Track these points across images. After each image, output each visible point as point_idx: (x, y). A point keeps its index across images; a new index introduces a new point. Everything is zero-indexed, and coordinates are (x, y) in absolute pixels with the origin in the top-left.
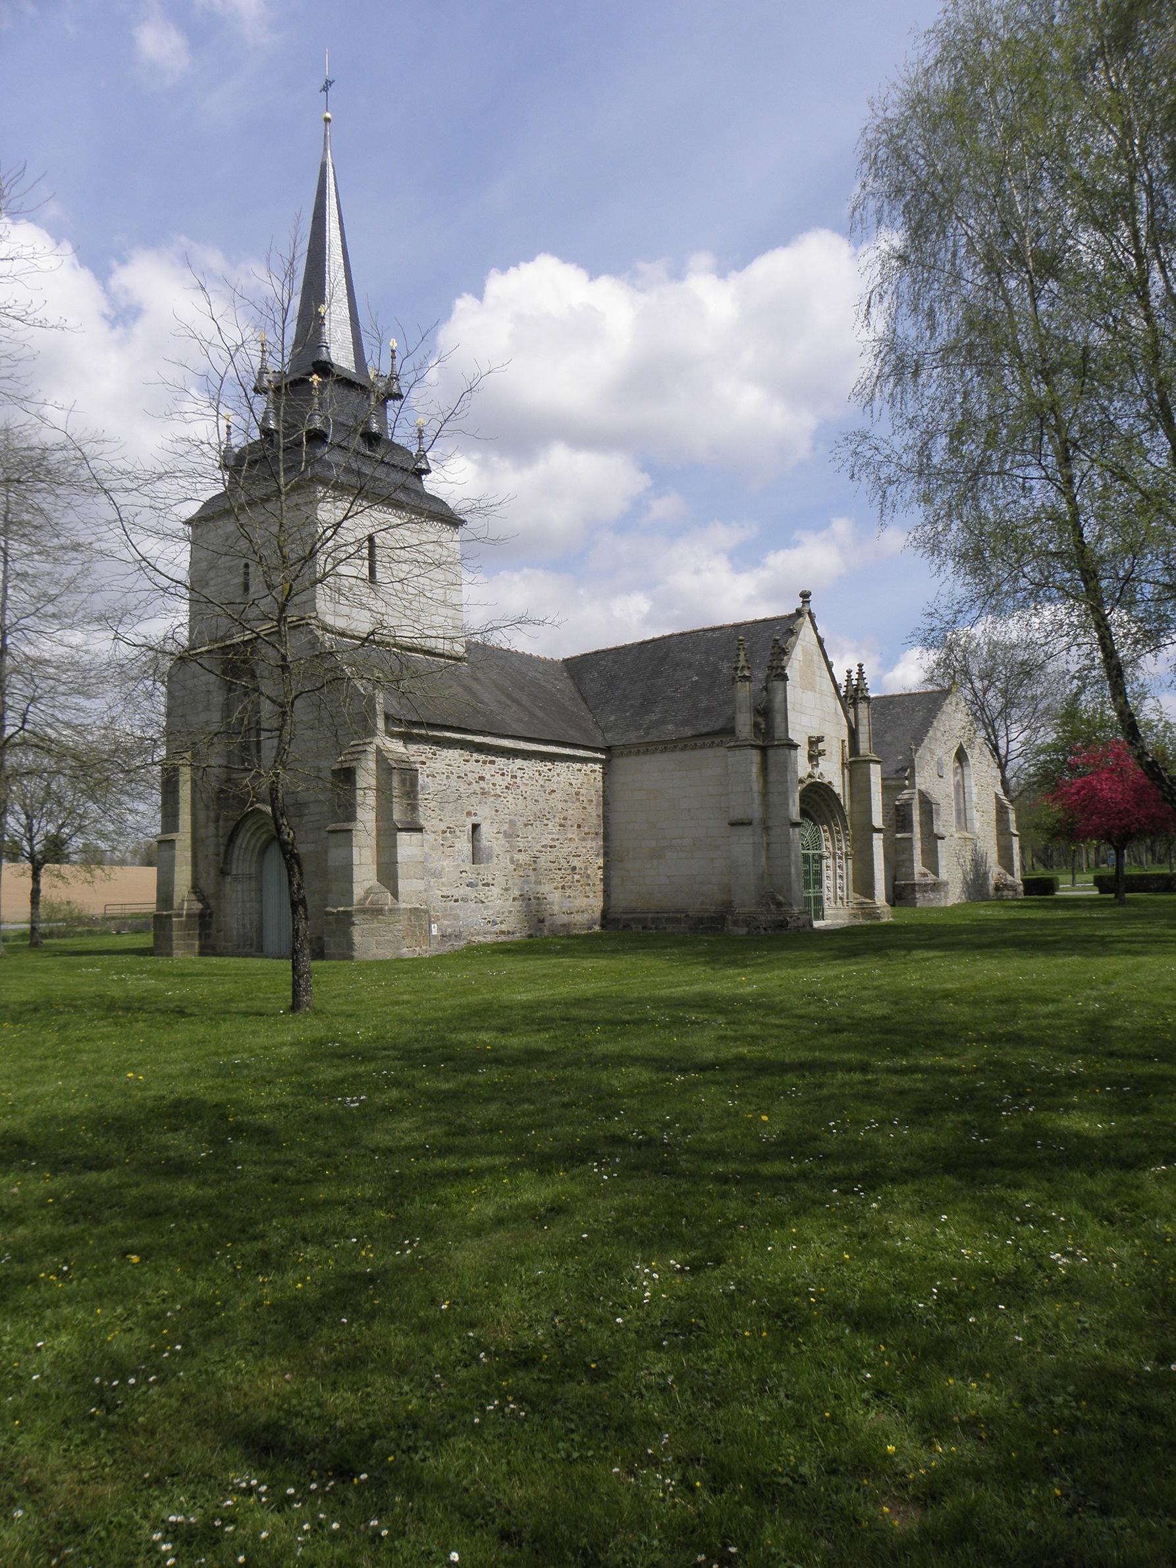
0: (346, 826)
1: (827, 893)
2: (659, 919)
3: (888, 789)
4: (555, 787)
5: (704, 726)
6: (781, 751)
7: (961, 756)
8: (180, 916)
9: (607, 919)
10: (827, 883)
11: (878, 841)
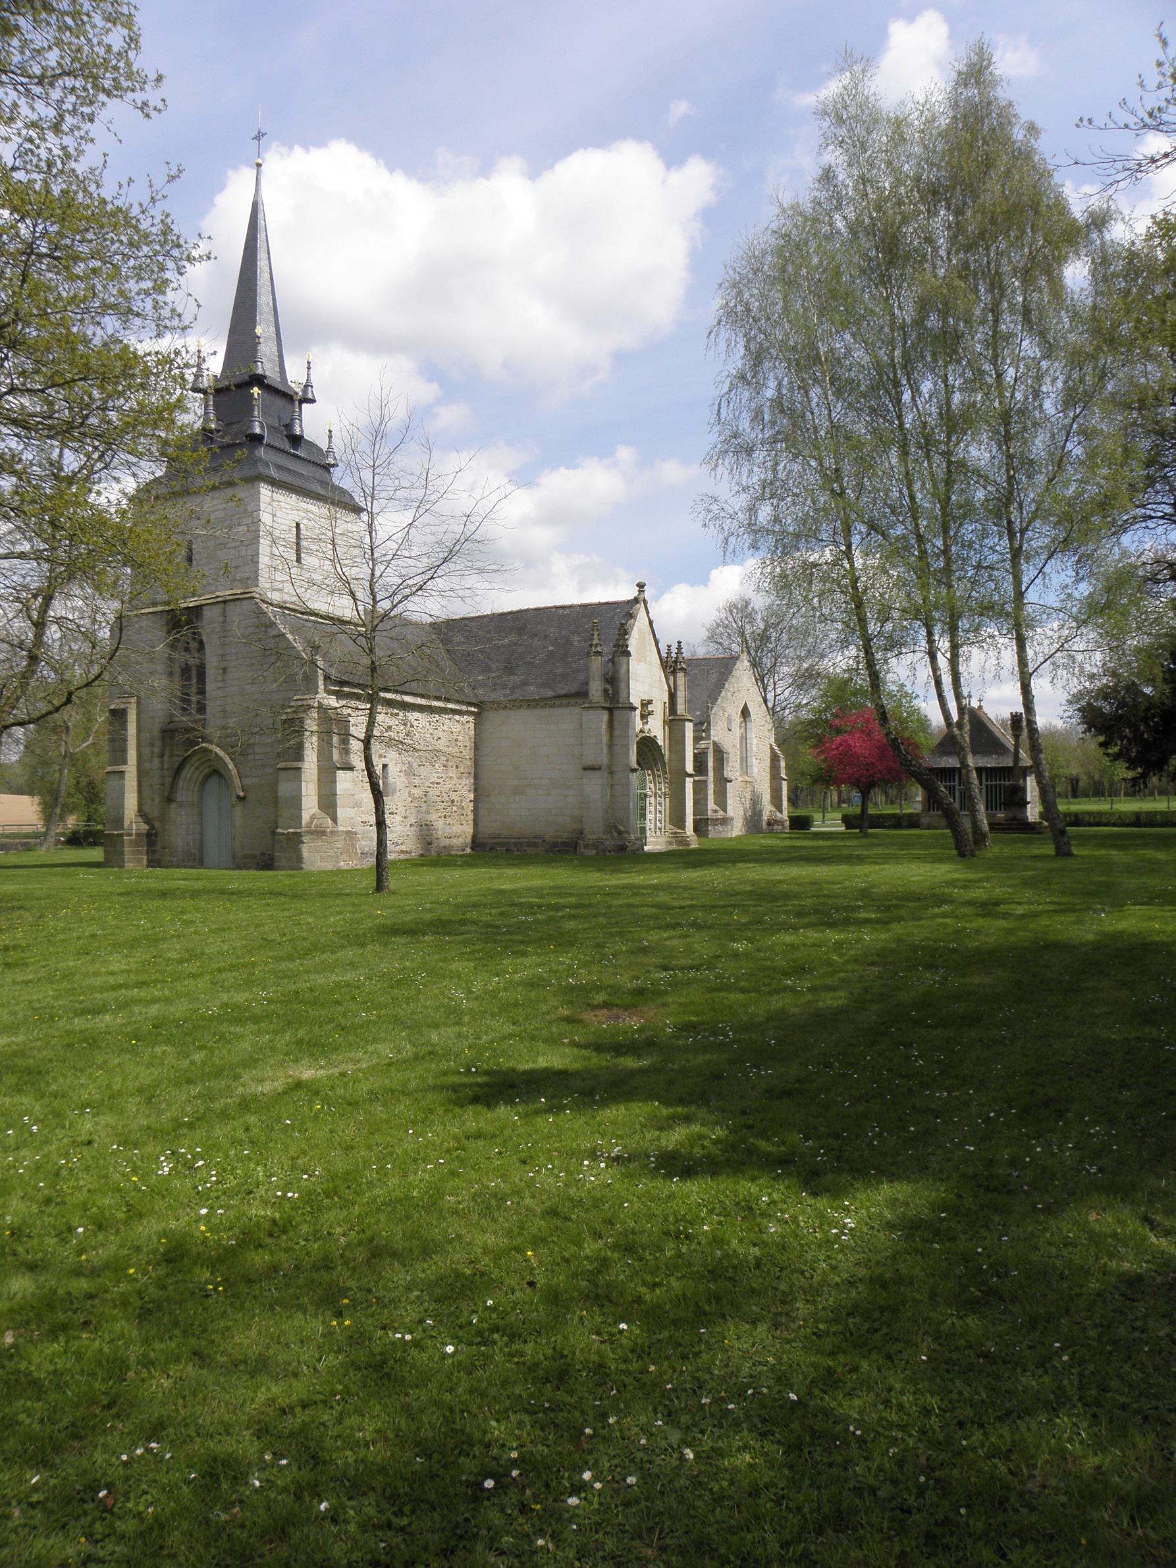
0: (295, 764)
1: (649, 825)
2: (520, 843)
3: (697, 739)
4: (440, 735)
5: (562, 689)
6: (624, 712)
7: (745, 713)
8: (130, 835)
9: (477, 843)
10: (649, 816)
11: (689, 782)
